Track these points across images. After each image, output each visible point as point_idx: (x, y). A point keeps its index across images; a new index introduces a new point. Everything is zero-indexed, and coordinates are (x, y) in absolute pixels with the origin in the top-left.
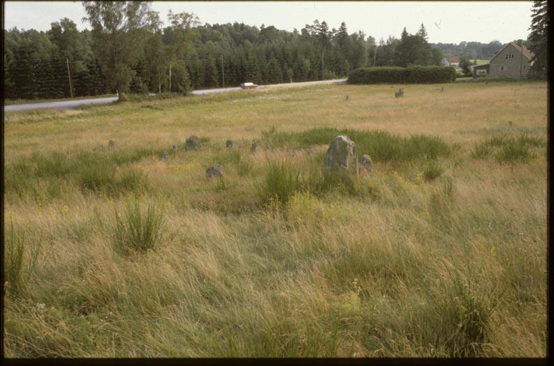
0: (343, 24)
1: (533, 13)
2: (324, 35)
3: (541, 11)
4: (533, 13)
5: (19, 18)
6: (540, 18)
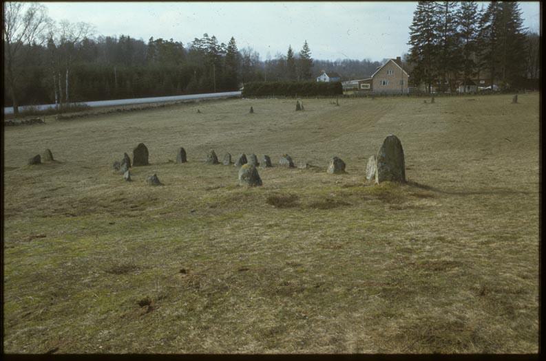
0: (233, 39)
1: (411, 31)
2: (214, 49)
4: (411, 31)
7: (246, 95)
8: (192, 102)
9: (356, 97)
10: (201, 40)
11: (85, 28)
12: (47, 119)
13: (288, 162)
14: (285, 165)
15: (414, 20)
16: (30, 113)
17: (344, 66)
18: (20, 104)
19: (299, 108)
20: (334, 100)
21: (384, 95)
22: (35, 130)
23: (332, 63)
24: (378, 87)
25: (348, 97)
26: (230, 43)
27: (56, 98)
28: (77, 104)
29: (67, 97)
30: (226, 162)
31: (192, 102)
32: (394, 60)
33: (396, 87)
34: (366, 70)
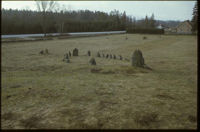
0: (125, 12)
1: (193, 10)
2: (118, 15)
3: (196, 10)
4: (193, 10)
5: (6, 6)
6: (196, 12)
7: (127, 33)
8: (107, 35)
9: (170, 35)
10: (113, 12)
11: (70, 7)
12: (54, 39)
13: (120, 58)
14: (119, 59)
15: (195, 5)
16: (50, 36)
17: (169, 23)
18: (47, 33)
19: (144, 38)
20: (159, 36)
21: (181, 34)
22: (49, 42)
23: (164, 22)
24: (179, 31)
25: (166, 35)
26: (124, 13)
27: (59, 31)
28: (66, 33)
29: (63, 31)
30: (102, 56)
31: (107, 35)
32: (186, 21)
33: (186, 32)
34: (174, 24)
